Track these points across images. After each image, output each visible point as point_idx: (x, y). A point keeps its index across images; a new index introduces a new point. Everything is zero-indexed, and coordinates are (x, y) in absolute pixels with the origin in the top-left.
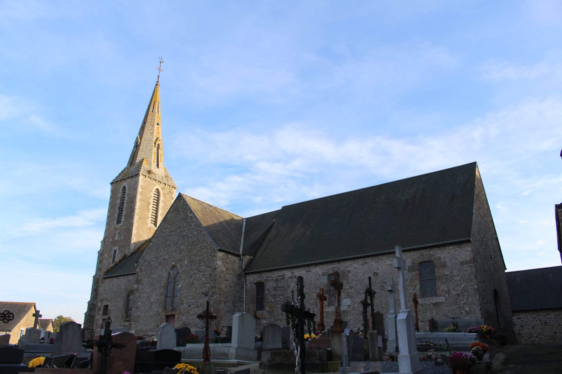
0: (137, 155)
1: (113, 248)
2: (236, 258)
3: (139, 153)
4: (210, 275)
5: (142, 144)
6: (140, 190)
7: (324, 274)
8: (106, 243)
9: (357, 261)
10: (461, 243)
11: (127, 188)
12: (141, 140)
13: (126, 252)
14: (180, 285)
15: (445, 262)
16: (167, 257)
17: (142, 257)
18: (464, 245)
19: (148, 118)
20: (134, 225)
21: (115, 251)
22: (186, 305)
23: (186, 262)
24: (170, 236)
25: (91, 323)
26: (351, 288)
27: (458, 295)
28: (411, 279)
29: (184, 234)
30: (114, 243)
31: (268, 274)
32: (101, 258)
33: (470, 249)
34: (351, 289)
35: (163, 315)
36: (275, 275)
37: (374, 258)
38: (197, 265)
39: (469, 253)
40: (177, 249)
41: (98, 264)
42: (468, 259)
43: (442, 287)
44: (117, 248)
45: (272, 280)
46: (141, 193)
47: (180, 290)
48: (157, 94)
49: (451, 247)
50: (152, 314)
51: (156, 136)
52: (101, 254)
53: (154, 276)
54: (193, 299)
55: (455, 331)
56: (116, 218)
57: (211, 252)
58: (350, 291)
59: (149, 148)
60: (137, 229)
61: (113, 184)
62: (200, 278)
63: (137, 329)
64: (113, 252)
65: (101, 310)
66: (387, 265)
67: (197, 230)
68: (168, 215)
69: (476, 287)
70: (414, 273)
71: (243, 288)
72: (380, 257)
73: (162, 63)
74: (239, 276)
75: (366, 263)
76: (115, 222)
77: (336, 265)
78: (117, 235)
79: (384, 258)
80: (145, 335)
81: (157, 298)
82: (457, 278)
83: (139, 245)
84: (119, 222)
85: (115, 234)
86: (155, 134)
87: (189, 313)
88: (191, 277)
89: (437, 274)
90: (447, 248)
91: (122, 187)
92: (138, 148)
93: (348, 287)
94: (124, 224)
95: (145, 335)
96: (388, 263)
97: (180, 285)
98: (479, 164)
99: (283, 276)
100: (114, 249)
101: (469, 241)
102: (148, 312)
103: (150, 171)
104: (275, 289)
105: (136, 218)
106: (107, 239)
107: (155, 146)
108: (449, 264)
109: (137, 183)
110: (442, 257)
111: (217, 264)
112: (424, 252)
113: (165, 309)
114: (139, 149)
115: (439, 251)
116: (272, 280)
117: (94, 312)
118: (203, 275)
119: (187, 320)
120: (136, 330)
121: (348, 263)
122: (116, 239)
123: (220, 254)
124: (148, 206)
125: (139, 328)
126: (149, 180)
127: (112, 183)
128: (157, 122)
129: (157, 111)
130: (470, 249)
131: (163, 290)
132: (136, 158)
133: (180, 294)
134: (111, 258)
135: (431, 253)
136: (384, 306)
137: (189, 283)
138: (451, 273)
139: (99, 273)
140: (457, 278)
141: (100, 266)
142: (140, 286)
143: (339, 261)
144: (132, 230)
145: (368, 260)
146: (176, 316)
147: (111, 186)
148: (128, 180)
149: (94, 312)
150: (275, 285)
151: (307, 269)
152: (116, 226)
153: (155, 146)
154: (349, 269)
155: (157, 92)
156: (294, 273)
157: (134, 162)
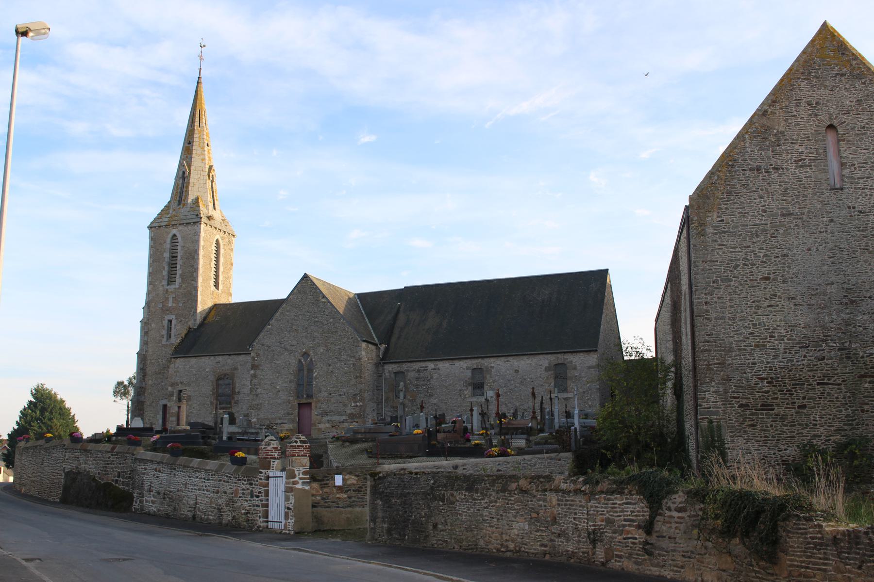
0: (187, 191)
1: (166, 317)
2: (372, 347)
3: (190, 188)
4: (354, 365)
5: (192, 176)
6: (202, 243)
7: (468, 368)
8: (151, 309)
9: (500, 358)
10: (590, 351)
11: (180, 240)
12: (190, 171)
13: (190, 323)
14: (316, 373)
15: (576, 365)
16: (294, 343)
17: (257, 341)
18: (592, 353)
19: (195, 136)
20: (199, 290)
21: (170, 321)
22: (325, 394)
23: (322, 350)
24: (297, 320)
25: (141, 410)
26: (494, 382)
27: (584, 392)
28: (547, 377)
29: (317, 320)
30: (166, 310)
31: (409, 365)
32: (146, 328)
33: (596, 356)
34: (494, 383)
35: (296, 403)
36: (417, 366)
37: (515, 357)
38: (337, 354)
39: (595, 360)
40: (309, 335)
41: (142, 337)
42: (594, 364)
43: (571, 385)
44: (172, 317)
45: (414, 370)
46: (203, 247)
47: (316, 378)
48: (201, 98)
49: (582, 354)
50: (279, 401)
51: (208, 164)
52: (145, 323)
53: (278, 362)
54: (333, 387)
55: (586, 419)
56: (166, 277)
57: (354, 341)
58: (493, 384)
59: (202, 182)
60: (202, 295)
61: (153, 229)
62: (341, 367)
63: (259, 417)
64: (166, 323)
65: (175, 396)
66: (528, 364)
67: (333, 318)
68: (291, 297)
69: (598, 387)
70: (550, 373)
71: (381, 376)
72: (521, 357)
73: (203, 48)
74: (377, 365)
75: (508, 361)
76: (165, 282)
77: (480, 360)
78: (171, 300)
79: (525, 358)
80: (272, 424)
81: (286, 385)
82: (584, 379)
83: (204, 313)
84: (171, 281)
85: (167, 299)
86: (207, 162)
87: (330, 401)
88: (330, 365)
89: (569, 375)
90: (578, 354)
91: (170, 235)
92: (186, 181)
93: (491, 381)
94: (181, 286)
95: (272, 424)
96: (528, 362)
97: (316, 373)
98: (610, 272)
99: (426, 369)
100: (168, 317)
101: (596, 351)
102: (273, 399)
103: (210, 217)
104: (417, 379)
105: (200, 280)
106: (153, 304)
107: (209, 179)
108: (579, 368)
109: (197, 234)
110: (574, 361)
111: (361, 354)
112: (560, 356)
113: (298, 396)
114: (188, 183)
115: (572, 356)
116: (414, 370)
117: (143, 397)
118: (345, 364)
119: (328, 407)
120: (258, 419)
121: (492, 360)
122: (170, 305)
123: (364, 345)
124: (210, 264)
125: (262, 416)
126: (210, 229)
127: (150, 228)
128: (206, 142)
129: (204, 125)
130: (596, 356)
131: (292, 377)
132: (187, 196)
133: (316, 382)
134: (164, 329)
135: (565, 357)
136: (523, 398)
137: (327, 372)
138: (580, 374)
139: (145, 348)
140: (584, 379)
141: (146, 338)
142: (258, 372)
143: (482, 358)
144: (196, 296)
145: (510, 358)
146: (313, 404)
147: (148, 231)
148: (180, 228)
149: (143, 397)
150: (417, 375)
151: (451, 362)
152: (168, 287)
153: (209, 179)
154: (492, 365)
155: (201, 95)
156: (437, 365)
157: (184, 201)
